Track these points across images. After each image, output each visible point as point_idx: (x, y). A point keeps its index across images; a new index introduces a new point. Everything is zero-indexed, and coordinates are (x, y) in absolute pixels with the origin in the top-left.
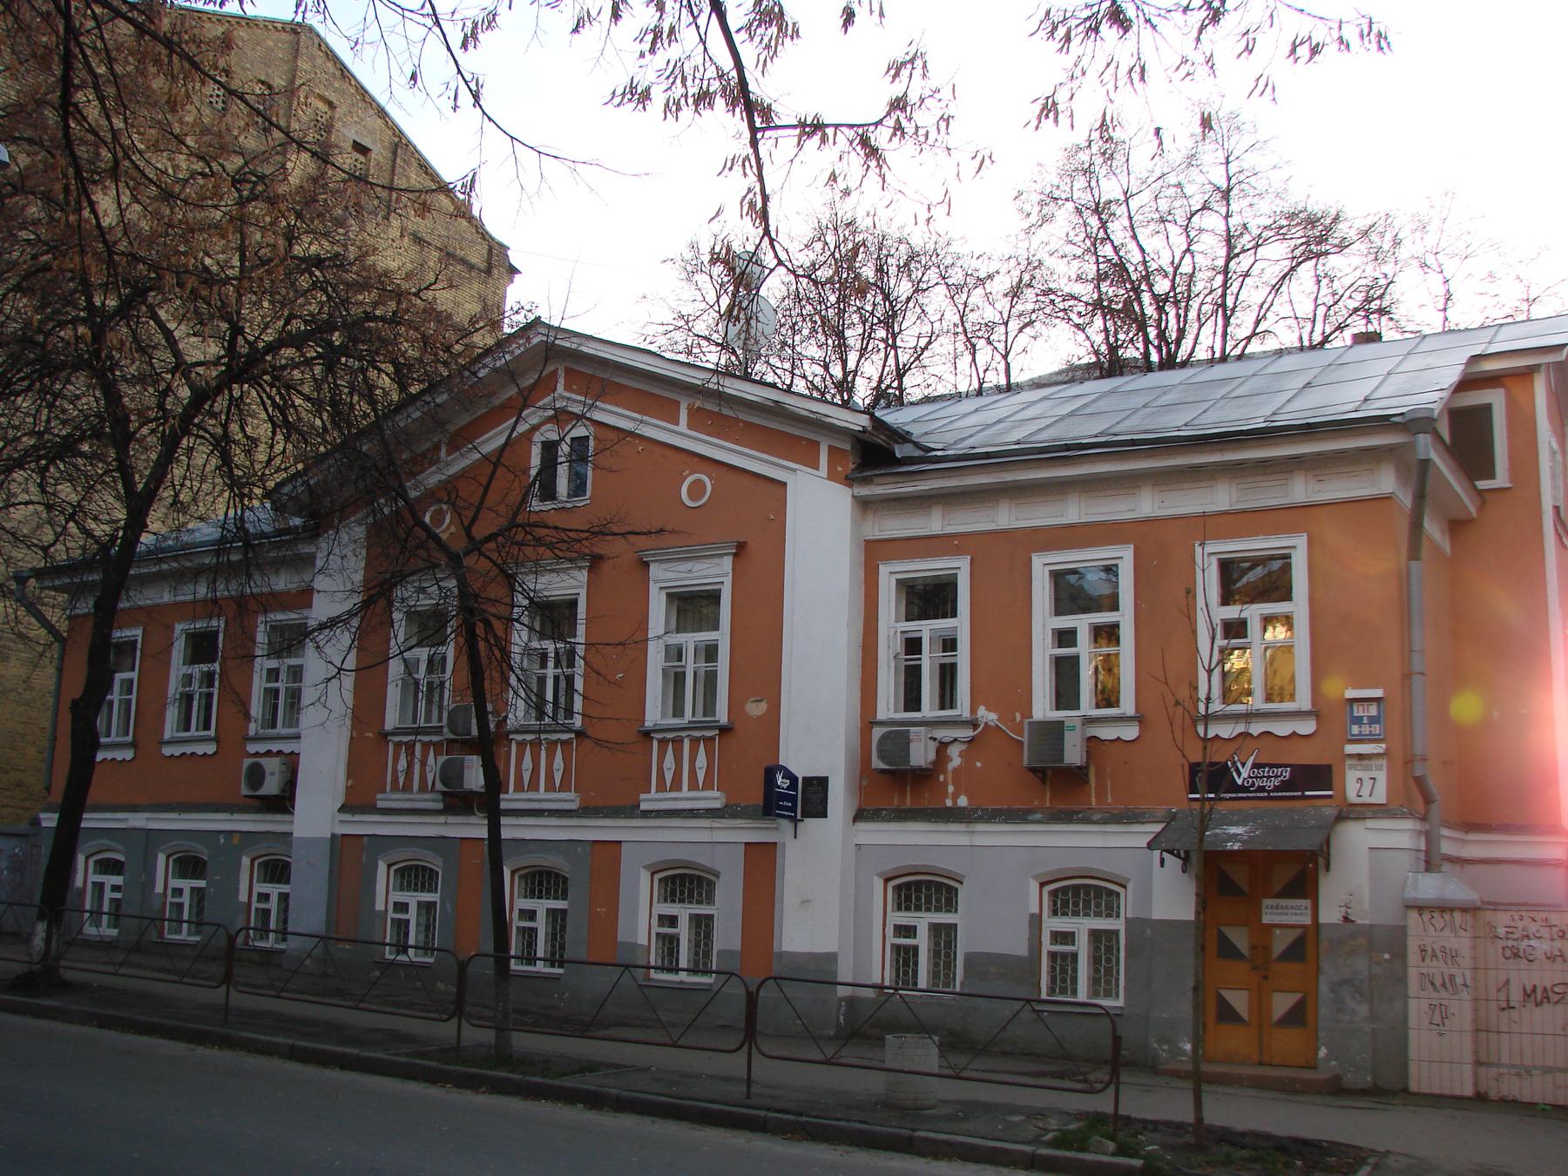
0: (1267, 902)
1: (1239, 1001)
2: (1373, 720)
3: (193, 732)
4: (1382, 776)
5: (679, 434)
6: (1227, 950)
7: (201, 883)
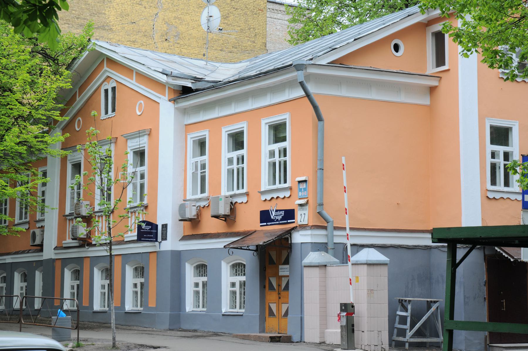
0: (280, 267)
1: (274, 307)
3: (24, 220)
4: (306, 212)
5: (132, 83)
6: (271, 288)
7: (143, 280)
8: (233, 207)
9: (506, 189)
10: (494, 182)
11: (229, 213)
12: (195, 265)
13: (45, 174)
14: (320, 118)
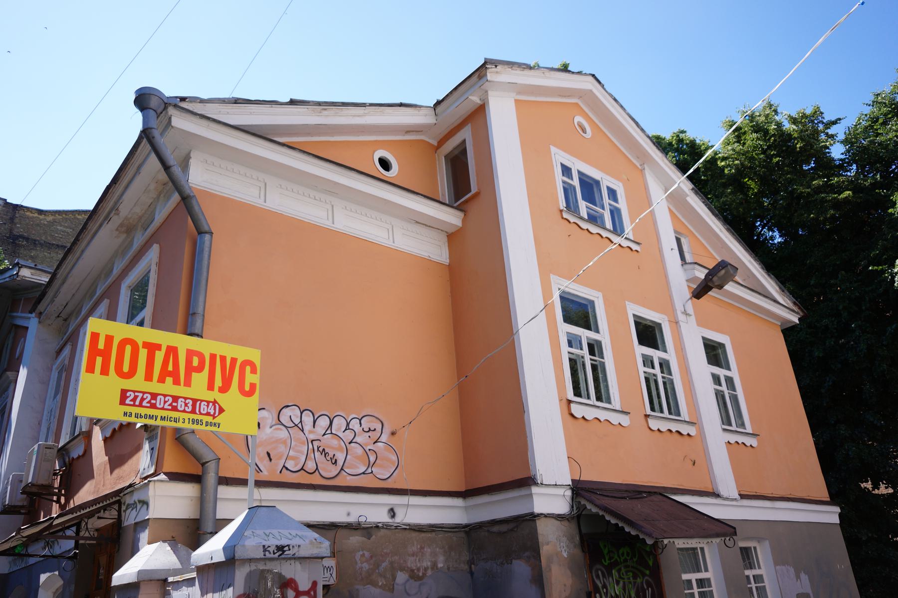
9: (599, 404)
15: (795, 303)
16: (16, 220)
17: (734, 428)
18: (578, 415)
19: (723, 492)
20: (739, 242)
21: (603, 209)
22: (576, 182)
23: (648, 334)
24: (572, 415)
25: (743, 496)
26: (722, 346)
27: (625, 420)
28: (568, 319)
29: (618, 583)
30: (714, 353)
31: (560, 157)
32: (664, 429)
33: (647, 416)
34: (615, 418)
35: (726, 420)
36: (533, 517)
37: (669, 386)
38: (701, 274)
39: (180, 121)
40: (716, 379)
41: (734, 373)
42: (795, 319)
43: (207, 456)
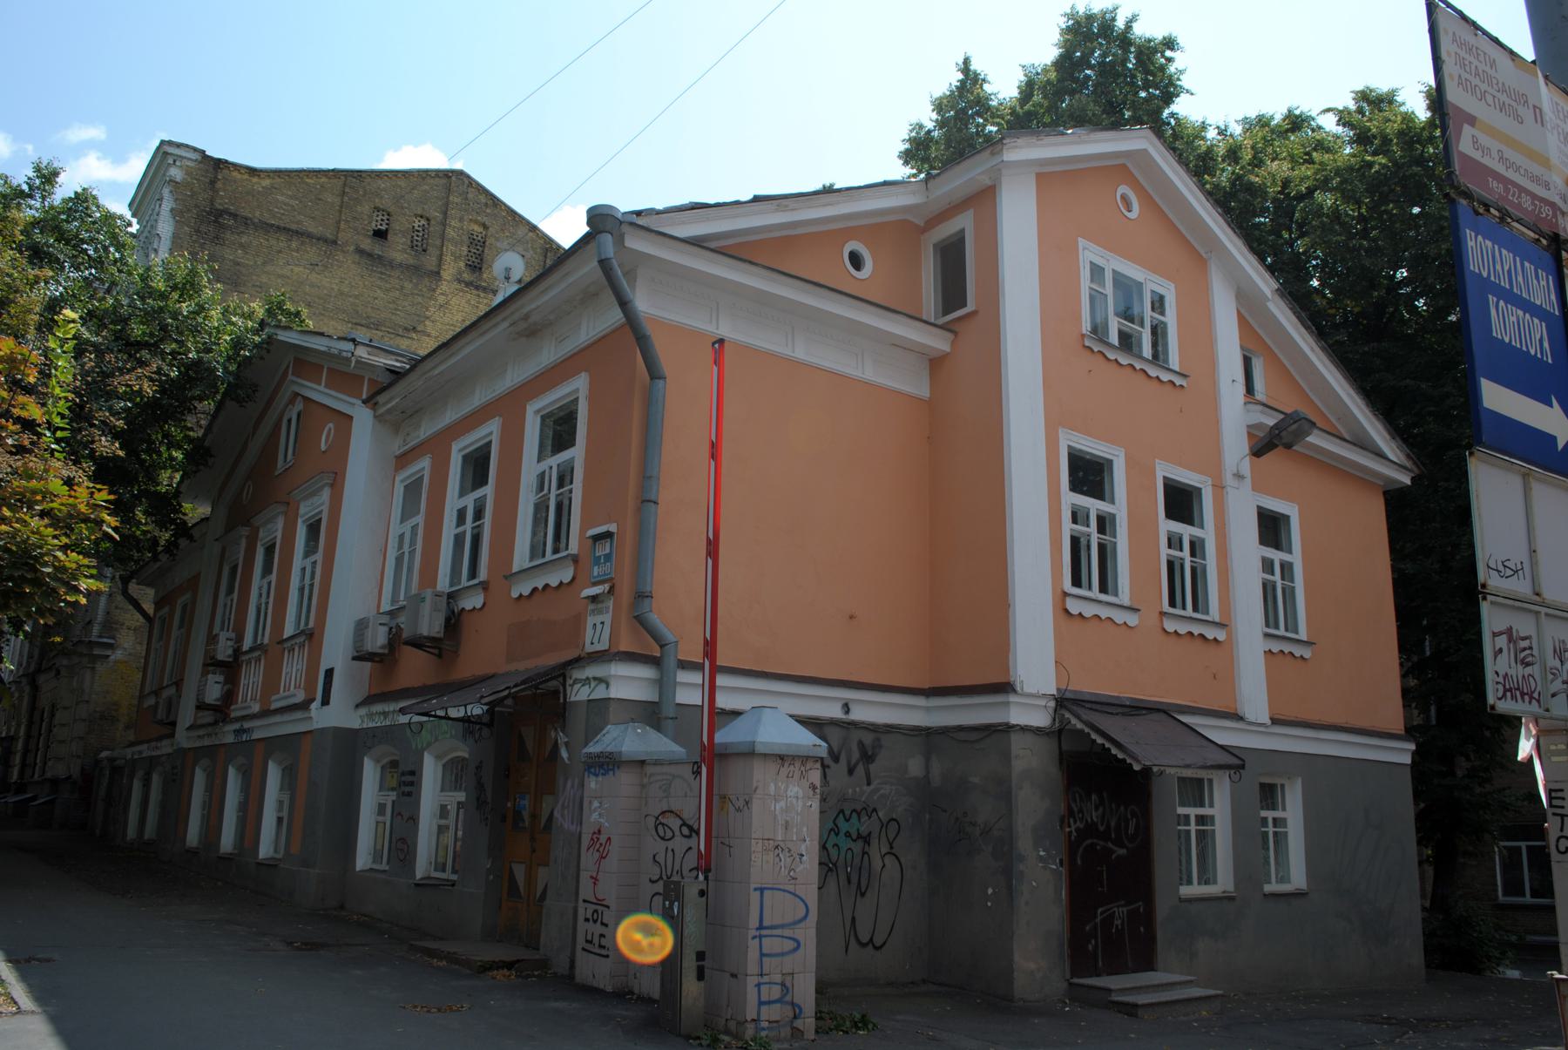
2: (608, 557)
8: (454, 622)
9: (1103, 597)
10: (1076, 582)
11: (441, 635)
12: (385, 761)
13: (814, 788)
14: (654, 373)
15: (1408, 456)
16: (219, 185)
17: (1281, 632)
18: (1074, 611)
19: (1250, 716)
20: (1337, 367)
21: (1142, 325)
22: (1109, 289)
23: (1181, 503)
24: (1066, 611)
25: (1275, 721)
26: (1287, 518)
27: (1132, 619)
28: (1076, 486)
29: (1097, 809)
30: (1272, 528)
31: (1090, 253)
32: (1182, 631)
33: (1162, 614)
34: (1119, 617)
35: (1270, 619)
36: (1007, 728)
37: (1198, 574)
38: (1270, 421)
39: (635, 243)
40: (1268, 565)
41: (1296, 558)
42: (1406, 480)
43: (670, 636)
